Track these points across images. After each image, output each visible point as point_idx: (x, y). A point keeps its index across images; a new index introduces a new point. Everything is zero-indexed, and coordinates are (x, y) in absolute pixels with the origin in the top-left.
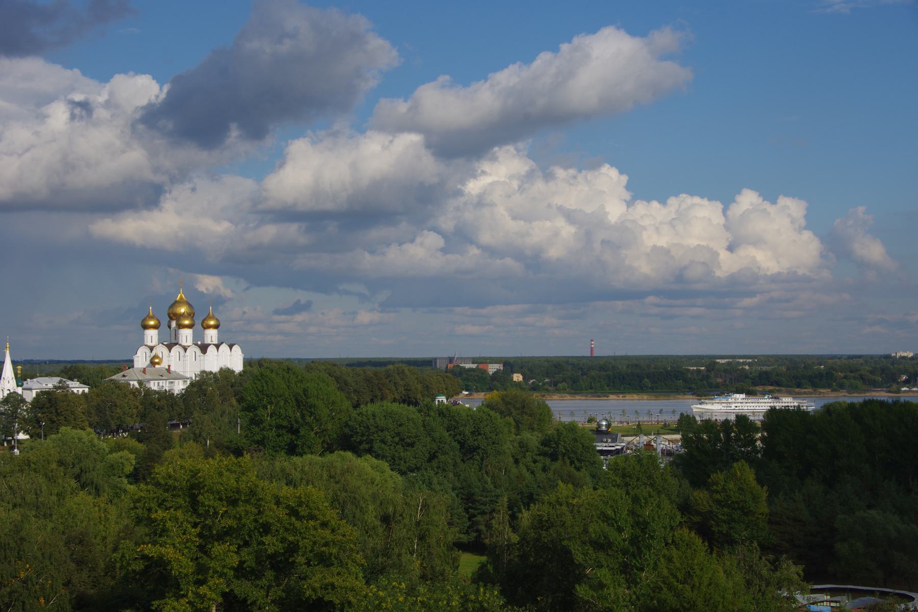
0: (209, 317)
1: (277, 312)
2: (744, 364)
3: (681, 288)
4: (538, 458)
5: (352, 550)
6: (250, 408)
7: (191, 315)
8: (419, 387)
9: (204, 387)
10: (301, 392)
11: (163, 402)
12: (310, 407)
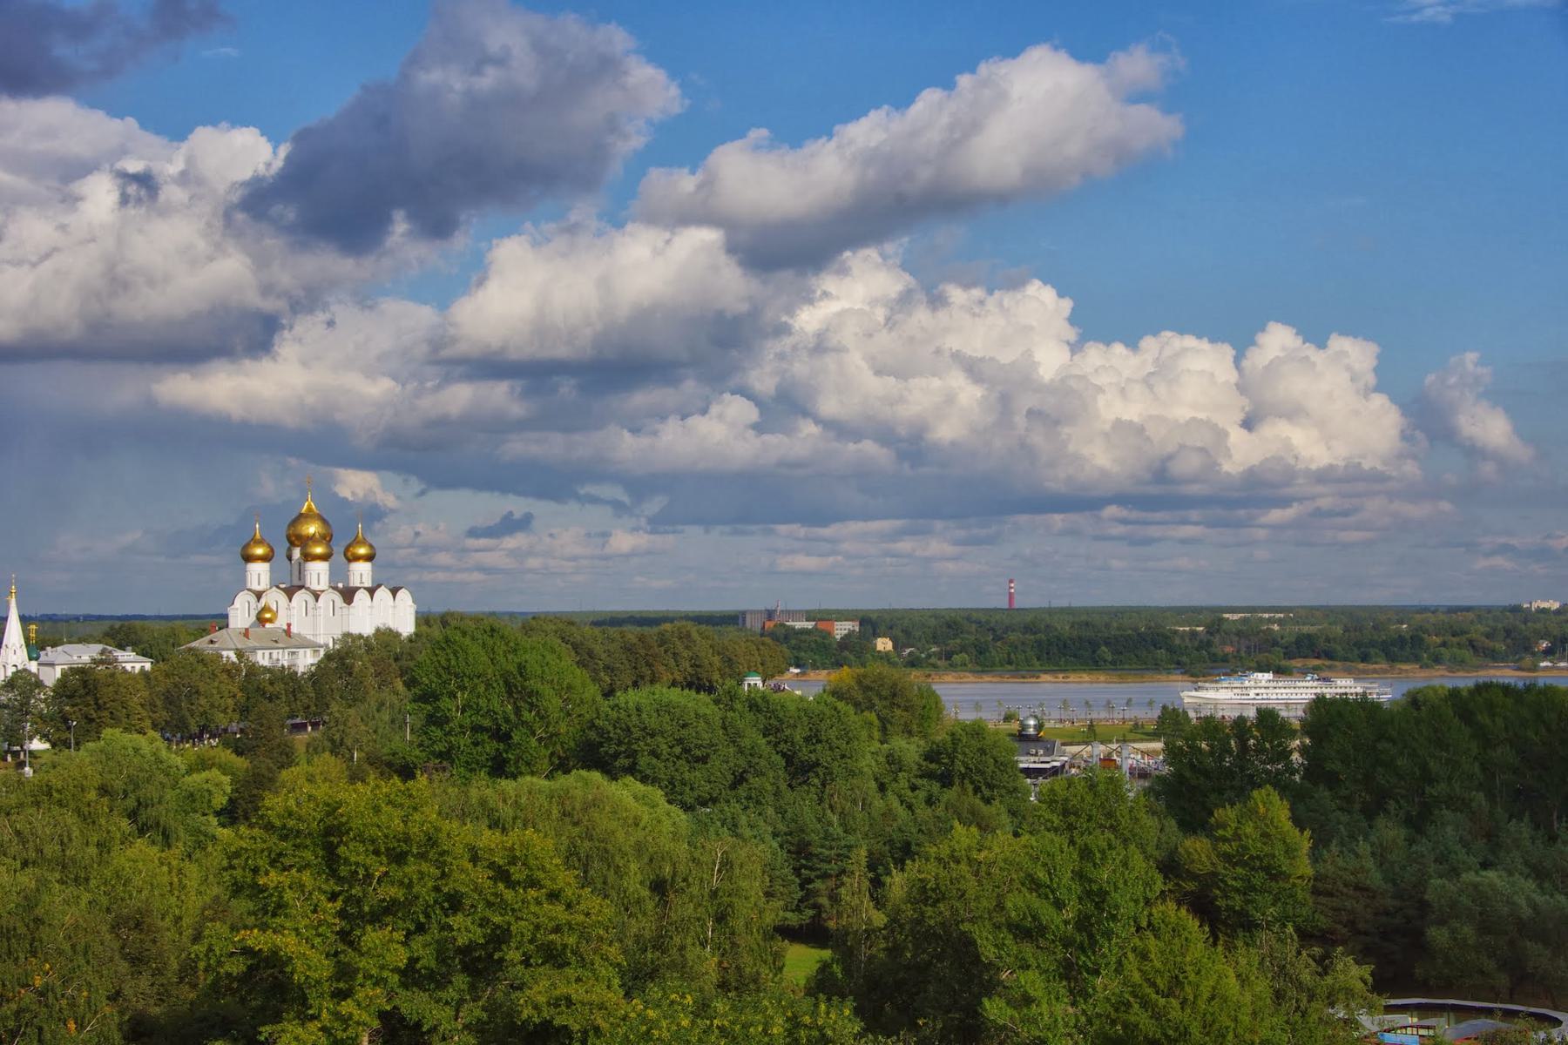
0: (357, 542)
1: (473, 533)
2: (1270, 621)
3: (1161, 493)
4: (919, 782)
5: (600, 939)
6: (427, 697)
7: (326, 538)
8: (716, 660)
9: (344, 660)
10: (513, 668)
11: (279, 687)
12: (530, 694)
